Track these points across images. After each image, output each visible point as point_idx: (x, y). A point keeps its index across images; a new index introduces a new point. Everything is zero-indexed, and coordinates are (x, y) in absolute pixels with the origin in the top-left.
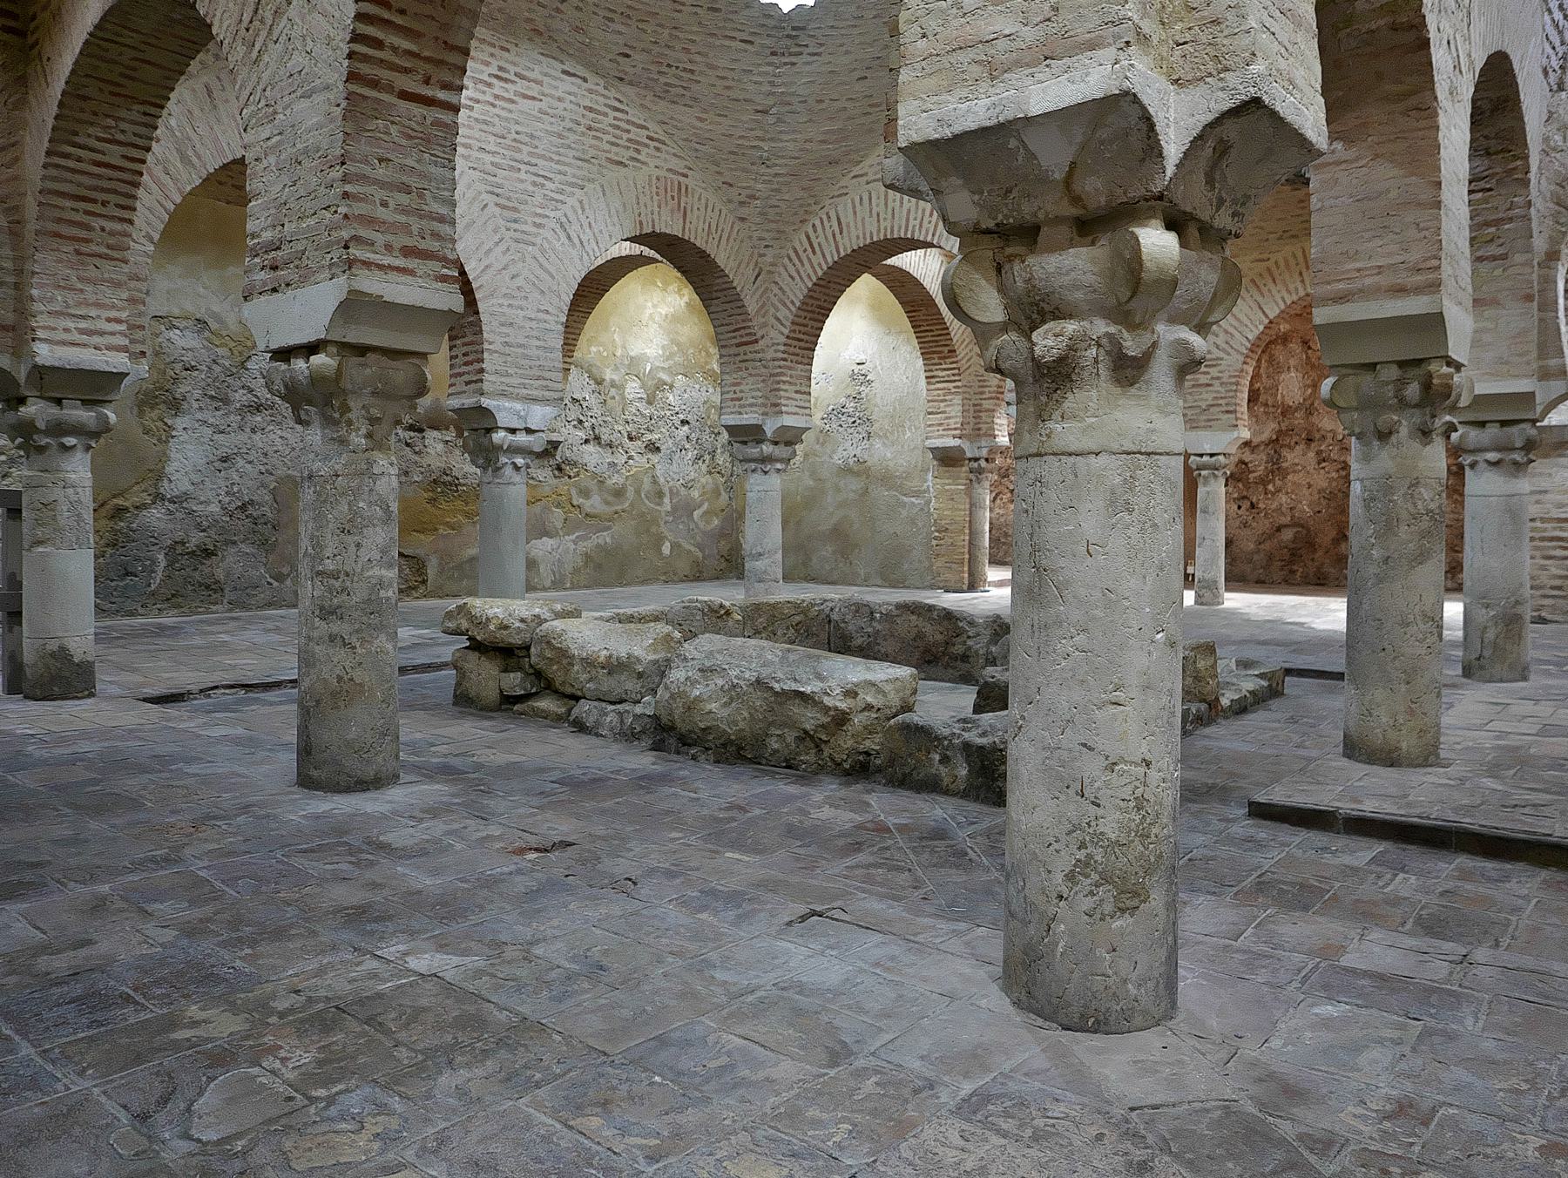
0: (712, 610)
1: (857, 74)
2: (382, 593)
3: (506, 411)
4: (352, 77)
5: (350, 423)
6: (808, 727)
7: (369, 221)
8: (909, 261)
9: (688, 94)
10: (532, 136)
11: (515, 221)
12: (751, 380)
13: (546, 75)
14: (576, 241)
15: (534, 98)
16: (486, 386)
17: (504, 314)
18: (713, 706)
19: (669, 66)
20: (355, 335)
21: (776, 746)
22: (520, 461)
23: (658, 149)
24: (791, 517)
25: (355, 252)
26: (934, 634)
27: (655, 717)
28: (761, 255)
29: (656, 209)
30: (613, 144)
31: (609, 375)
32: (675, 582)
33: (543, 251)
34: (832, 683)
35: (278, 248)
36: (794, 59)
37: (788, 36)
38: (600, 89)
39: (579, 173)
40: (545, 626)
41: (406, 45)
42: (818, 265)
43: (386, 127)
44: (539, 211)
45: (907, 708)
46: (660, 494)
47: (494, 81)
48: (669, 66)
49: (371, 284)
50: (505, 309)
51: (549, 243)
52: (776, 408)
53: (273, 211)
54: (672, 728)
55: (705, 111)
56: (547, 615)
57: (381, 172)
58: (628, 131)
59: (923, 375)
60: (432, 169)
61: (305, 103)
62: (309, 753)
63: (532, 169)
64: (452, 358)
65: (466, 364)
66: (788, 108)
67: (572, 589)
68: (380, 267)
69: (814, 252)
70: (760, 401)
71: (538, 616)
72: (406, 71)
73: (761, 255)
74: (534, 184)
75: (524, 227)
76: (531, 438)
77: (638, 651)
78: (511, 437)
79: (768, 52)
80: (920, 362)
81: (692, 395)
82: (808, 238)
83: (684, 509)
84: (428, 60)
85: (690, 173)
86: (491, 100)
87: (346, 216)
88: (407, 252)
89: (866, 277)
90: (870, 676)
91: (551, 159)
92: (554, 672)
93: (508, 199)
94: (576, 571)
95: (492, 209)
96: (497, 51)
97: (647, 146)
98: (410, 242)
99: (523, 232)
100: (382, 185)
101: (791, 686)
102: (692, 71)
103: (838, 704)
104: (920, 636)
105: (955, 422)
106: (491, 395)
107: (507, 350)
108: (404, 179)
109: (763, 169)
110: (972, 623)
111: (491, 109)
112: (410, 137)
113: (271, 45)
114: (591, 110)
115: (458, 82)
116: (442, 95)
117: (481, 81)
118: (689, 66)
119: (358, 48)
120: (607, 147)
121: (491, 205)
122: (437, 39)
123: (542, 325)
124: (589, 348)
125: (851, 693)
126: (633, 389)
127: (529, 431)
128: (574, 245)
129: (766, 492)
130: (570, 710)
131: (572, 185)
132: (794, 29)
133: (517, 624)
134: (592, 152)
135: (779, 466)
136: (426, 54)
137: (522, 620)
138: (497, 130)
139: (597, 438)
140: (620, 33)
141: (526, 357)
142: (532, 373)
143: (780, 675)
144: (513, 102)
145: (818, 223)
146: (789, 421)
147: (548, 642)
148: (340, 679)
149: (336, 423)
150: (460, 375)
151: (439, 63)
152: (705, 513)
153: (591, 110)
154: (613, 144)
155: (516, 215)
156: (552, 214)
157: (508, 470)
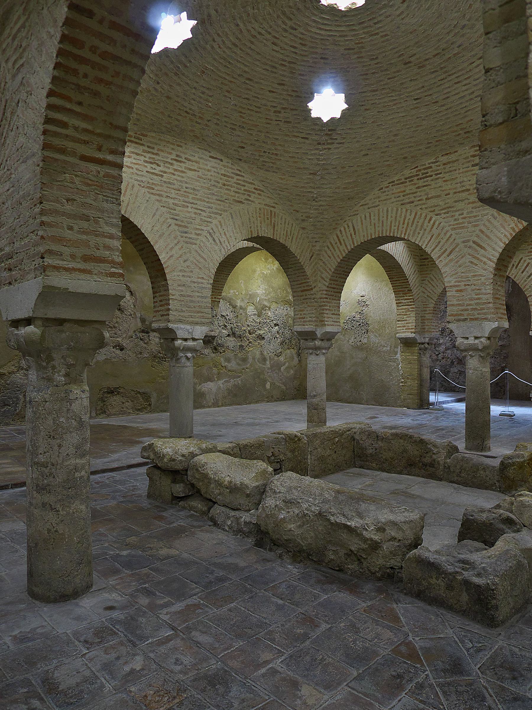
0: (291, 439)
1: (363, 153)
2: (77, 475)
3: (182, 330)
4: (46, 146)
5: (54, 367)
6: (353, 549)
7: (60, 240)
8: (389, 248)
9: (275, 166)
10: (194, 189)
11: (186, 233)
12: (309, 308)
13: (201, 158)
14: (218, 241)
15: (195, 170)
16: (171, 318)
17: (180, 280)
18: (292, 526)
19: (265, 152)
20: (53, 313)
21: (332, 557)
22: (189, 355)
23: (259, 194)
24: (330, 370)
25: (48, 261)
26: (413, 451)
27: (257, 525)
28: (313, 246)
29: (259, 225)
30: (236, 192)
31: (239, 303)
32: (272, 401)
33: (200, 247)
34: (368, 521)
35: (12, 258)
36: (329, 146)
37: (326, 134)
38: (230, 165)
39: (218, 207)
40: (196, 459)
41: (84, 125)
42: (342, 251)
43: (72, 179)
44: (198, 227)
45: (416, 543)
46: (264, 359)
47: (174, 162)
48: (265, 152)
49: (59, 280)
50: (182, 278)
51: (204, 243)
52: (322, 323)
53: (9, 234)
54: (267, 533)
55: (284, 174)
56: (197, 452)
57: (68, 207)
58: (244, 186)
59: (395, 302)
60: (105, 205)
61: (24, 166)
62: (32, 576)
63: (194, 206)
64: (154, 302)
65: (161, 306)
66: (326, 172)
67: (222, 406)
68: (66, 269)
69: (341, 244)
70: (314, 319)
71: (192, 453)
72: (86, 142)
73: (313, 246)
74: (195, 213)
75: (190, 236)
76: (195, 343)
77: (246, 481)
78: (184, 343)
79: (316, 143)
80: (393, 295)
81: (279, 312)
82: (338, 237)
83: (276, 366)
84: (99, 135)
85: (276, 206)
86: (173, 172)
87: (42, 237)
88: (86, 259)
89: (368, 256)
90: (392, 517)
91: (204, 201)
92: (200, 485)
93: (182, 221)
94: (225, 397)
95: (173, 227)
96: (175, 147)
97: (254, 193)
98: (88, 252)
99: (190, 238)
100: (70, 216)
101: (342, 520)
102: (276, 154)
103: (373, 537)
104: (405, 451)
105: (412, 325)
106: (175, 322)
107: (182, 298)
108: (85, 212)
109: (314, 203)
110: (435, 446)
111: (173, 176)
112: (88, 185)
113: (10, 133)
114: (224, 175)
115: (120, 149)
116: (110, 158)
117: (167, 162)
118: (275, 152)
119: (51, 128)
120: (233, 194)
121: (173, 225)
122: (105, 121)
123: (200, 285)
124: (228, 291)
125: (381, 529)
126: (251, 310)
127: (194, 339)
128: (217, 244)
129: (317, 365)
130: (209, 509)
131: (216, 213)
132: (329, 130)
133: (180, 458)
134: (225, 197)
135: (324, 351)
136: (98, 131)
137: (183, 456)
138: (176, 187)
139: (234, 334)
140: (239, 136)
141: (192, 301)
142: (193, 309)
143: (333, 510)
144: (184, 172)
145: (342, 229)
146: (329, 329)
147: (197, 470)
148: (49, 531)
149: (45, 368)
150: (158, 311)
151: (108, 137)
152: (286, 368)
153: (224, 175)
154: (236, 192)
155: (186, 230)
156: (205, 229)
157: (183, 360)
